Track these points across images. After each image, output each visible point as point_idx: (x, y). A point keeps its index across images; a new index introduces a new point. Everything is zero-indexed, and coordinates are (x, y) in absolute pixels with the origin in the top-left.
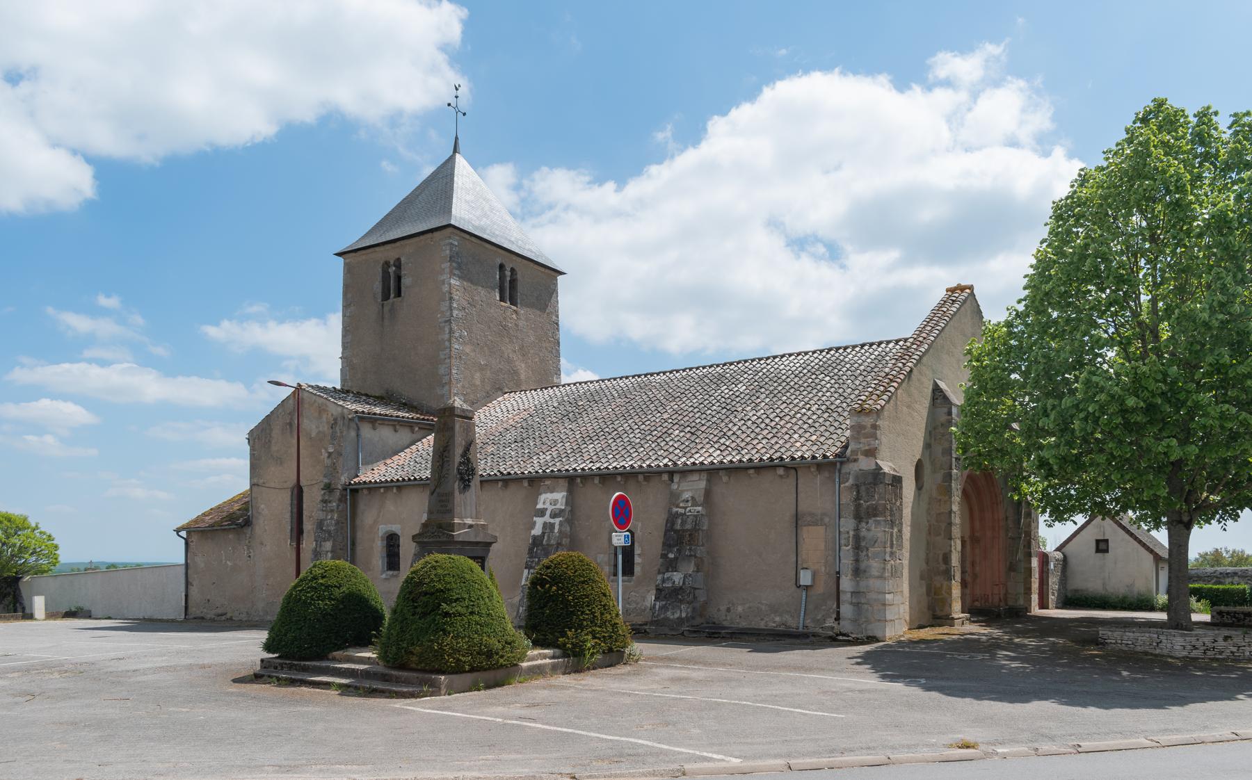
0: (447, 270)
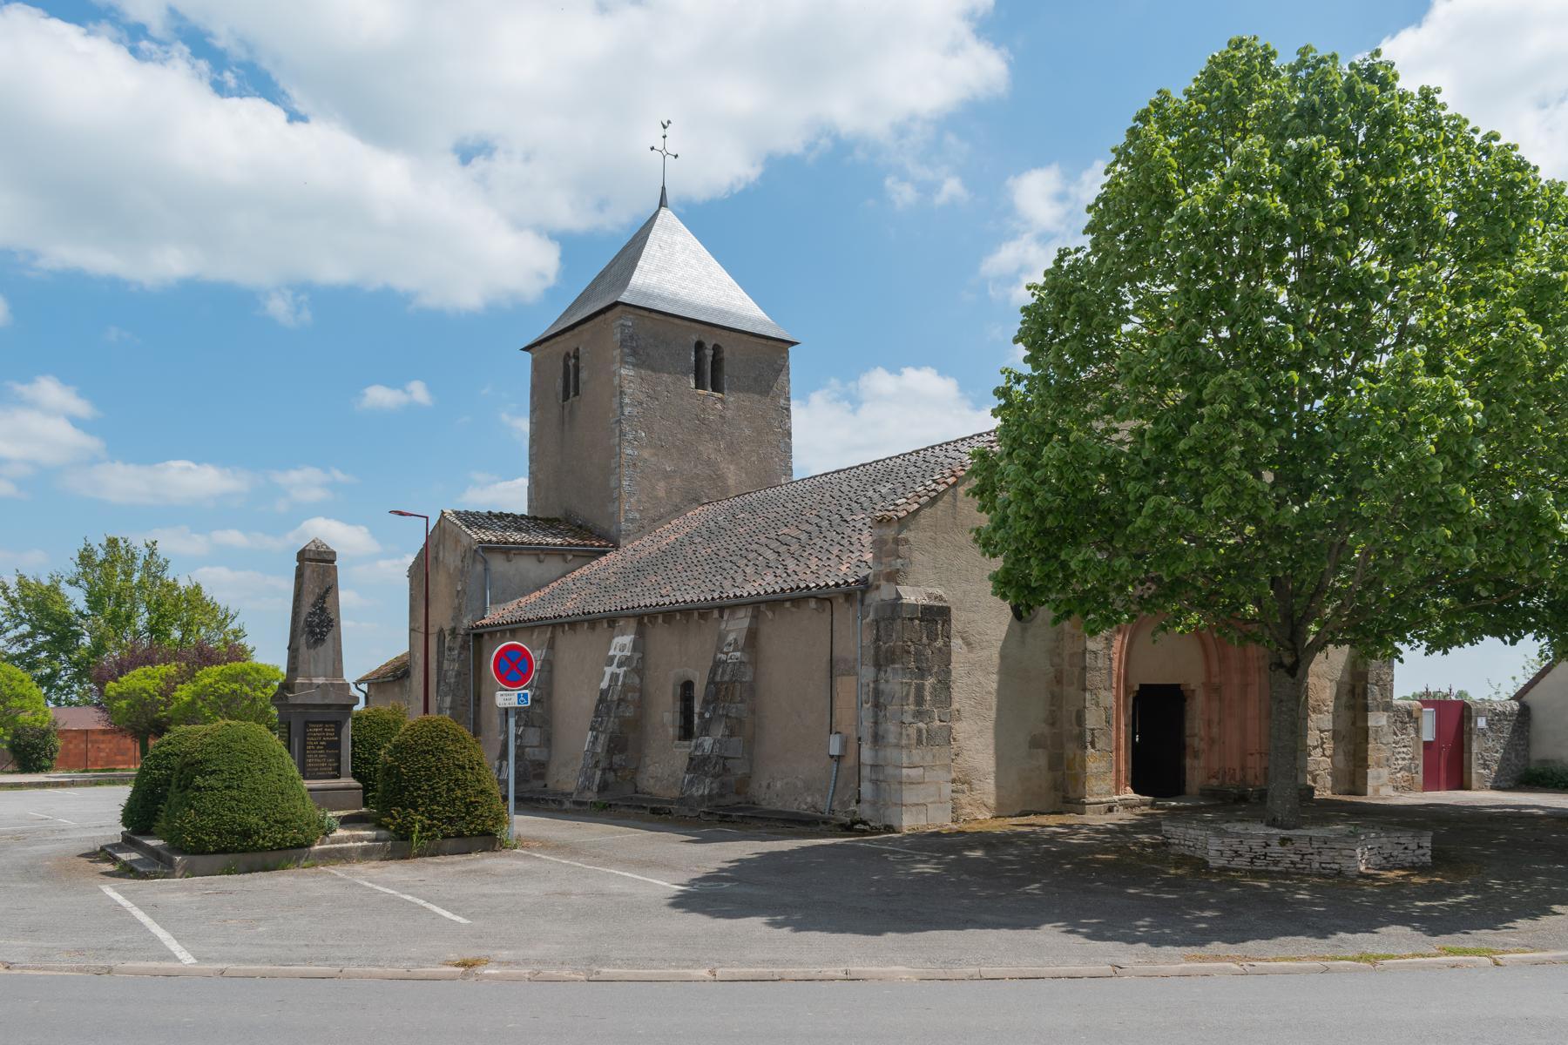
0: (618, 358)
